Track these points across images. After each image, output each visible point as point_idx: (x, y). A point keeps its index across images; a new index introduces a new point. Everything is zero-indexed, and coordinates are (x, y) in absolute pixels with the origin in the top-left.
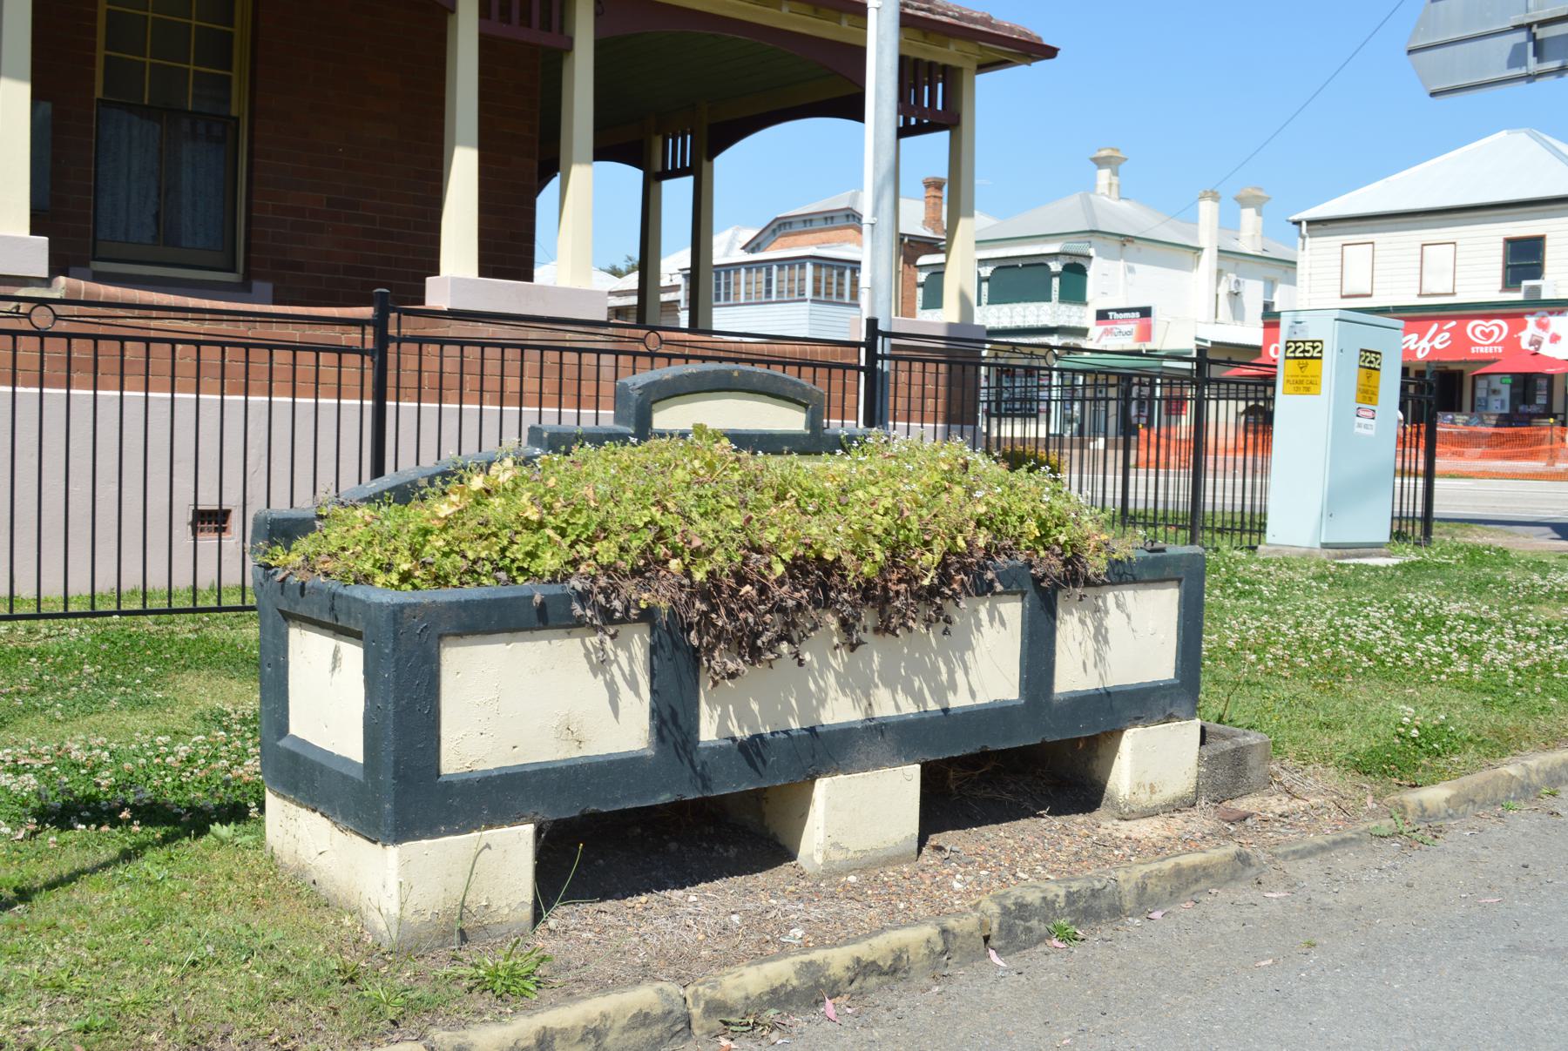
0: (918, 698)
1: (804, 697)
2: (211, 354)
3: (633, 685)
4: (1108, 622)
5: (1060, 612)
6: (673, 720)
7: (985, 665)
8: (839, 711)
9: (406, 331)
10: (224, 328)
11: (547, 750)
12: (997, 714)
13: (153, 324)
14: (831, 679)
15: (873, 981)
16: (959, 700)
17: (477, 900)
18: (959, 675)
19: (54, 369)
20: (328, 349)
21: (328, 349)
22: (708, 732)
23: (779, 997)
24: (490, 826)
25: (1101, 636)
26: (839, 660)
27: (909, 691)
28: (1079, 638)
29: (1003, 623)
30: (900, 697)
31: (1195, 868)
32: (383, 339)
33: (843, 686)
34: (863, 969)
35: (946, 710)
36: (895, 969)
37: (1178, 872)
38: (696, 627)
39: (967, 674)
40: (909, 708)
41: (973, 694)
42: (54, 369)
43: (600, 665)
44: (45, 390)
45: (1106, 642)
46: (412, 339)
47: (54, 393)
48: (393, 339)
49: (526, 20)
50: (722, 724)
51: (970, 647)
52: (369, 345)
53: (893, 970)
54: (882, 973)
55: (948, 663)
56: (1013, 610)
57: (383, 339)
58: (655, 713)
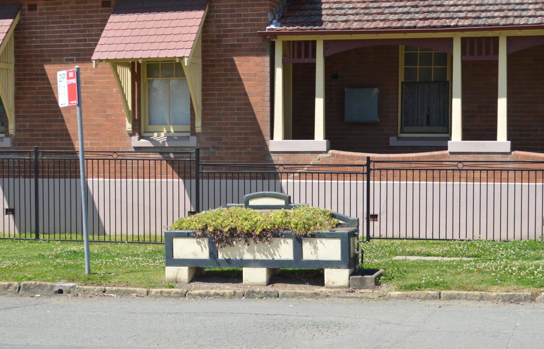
0: (266, 256)
1: (239, 253)
2: (518, 173)
3: (205, 247)
4: (317, 245)
5: (303, 242)
6: (213, 254)
7: (284, 251)
8: (247, 256)
9: (376, 167)
10: (413, 165)
11: (191, 257)
12: (287, 262)
13: (488, 166)
14: (245, 250)
15: (218, 296)
16: (277, 258)
17: (178, 277)
18: (276, 252)
19: (384, 177)
20: (540, 170)
21: (540, 170)
22: (220, 257)
23: (201, 295)
24: (181, 266)
25: (315, 248)
26: (246, 247)
27: (264, 254)
28: (309, 248)
29: (287, 243)
30: (262, 255)
31: (300, 293)
32: (369, 170)
33: (248, 251)
34: (216, 294)
35: (241, 259)
36: (223, 296)
37: (295, 293)
38: (218, 238)
39: (278, 252)
40: (264, 258)
41: (280, 257)
42: (384, 177)
43: (199, 243)
44: (320, 181)
45: (317, 249)
46: (378, 169)
47: (410, 183)
48: (372, 169)
49: (480, 53)
50: (223, 256)
51: (279, 247)
52: (365, 171)
53: (223, 296)
54: (220, 295)
55: (273, 250)
56: (290, 241)
57: (369, 170)
58: (210, 252)
